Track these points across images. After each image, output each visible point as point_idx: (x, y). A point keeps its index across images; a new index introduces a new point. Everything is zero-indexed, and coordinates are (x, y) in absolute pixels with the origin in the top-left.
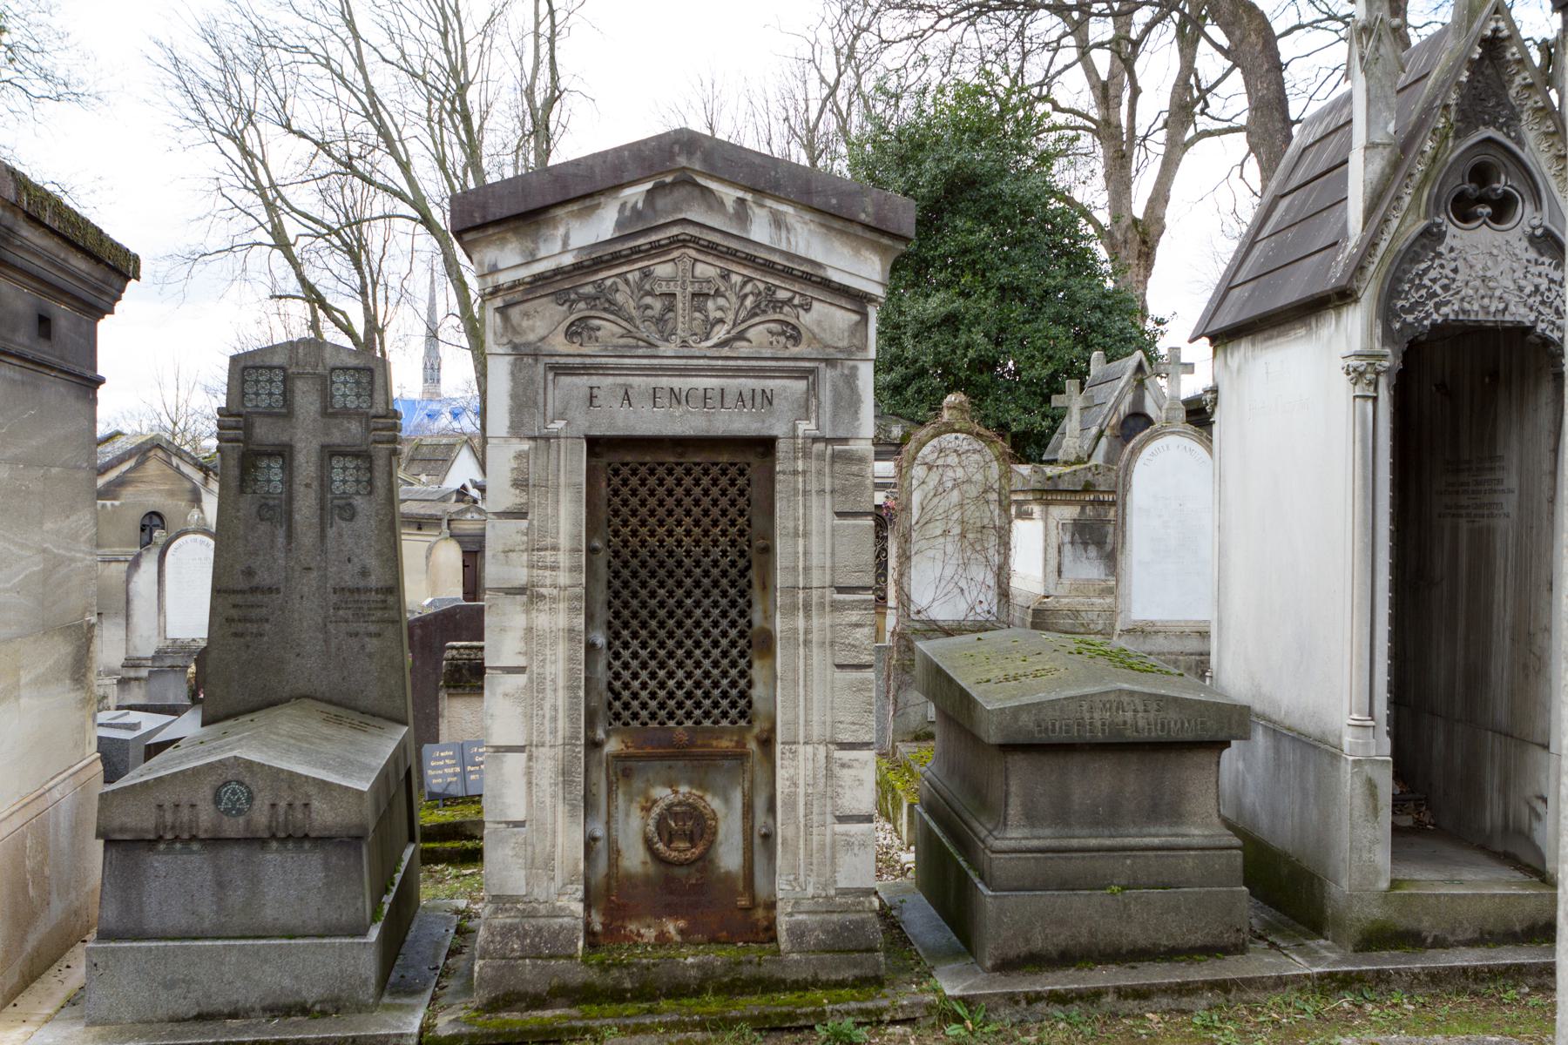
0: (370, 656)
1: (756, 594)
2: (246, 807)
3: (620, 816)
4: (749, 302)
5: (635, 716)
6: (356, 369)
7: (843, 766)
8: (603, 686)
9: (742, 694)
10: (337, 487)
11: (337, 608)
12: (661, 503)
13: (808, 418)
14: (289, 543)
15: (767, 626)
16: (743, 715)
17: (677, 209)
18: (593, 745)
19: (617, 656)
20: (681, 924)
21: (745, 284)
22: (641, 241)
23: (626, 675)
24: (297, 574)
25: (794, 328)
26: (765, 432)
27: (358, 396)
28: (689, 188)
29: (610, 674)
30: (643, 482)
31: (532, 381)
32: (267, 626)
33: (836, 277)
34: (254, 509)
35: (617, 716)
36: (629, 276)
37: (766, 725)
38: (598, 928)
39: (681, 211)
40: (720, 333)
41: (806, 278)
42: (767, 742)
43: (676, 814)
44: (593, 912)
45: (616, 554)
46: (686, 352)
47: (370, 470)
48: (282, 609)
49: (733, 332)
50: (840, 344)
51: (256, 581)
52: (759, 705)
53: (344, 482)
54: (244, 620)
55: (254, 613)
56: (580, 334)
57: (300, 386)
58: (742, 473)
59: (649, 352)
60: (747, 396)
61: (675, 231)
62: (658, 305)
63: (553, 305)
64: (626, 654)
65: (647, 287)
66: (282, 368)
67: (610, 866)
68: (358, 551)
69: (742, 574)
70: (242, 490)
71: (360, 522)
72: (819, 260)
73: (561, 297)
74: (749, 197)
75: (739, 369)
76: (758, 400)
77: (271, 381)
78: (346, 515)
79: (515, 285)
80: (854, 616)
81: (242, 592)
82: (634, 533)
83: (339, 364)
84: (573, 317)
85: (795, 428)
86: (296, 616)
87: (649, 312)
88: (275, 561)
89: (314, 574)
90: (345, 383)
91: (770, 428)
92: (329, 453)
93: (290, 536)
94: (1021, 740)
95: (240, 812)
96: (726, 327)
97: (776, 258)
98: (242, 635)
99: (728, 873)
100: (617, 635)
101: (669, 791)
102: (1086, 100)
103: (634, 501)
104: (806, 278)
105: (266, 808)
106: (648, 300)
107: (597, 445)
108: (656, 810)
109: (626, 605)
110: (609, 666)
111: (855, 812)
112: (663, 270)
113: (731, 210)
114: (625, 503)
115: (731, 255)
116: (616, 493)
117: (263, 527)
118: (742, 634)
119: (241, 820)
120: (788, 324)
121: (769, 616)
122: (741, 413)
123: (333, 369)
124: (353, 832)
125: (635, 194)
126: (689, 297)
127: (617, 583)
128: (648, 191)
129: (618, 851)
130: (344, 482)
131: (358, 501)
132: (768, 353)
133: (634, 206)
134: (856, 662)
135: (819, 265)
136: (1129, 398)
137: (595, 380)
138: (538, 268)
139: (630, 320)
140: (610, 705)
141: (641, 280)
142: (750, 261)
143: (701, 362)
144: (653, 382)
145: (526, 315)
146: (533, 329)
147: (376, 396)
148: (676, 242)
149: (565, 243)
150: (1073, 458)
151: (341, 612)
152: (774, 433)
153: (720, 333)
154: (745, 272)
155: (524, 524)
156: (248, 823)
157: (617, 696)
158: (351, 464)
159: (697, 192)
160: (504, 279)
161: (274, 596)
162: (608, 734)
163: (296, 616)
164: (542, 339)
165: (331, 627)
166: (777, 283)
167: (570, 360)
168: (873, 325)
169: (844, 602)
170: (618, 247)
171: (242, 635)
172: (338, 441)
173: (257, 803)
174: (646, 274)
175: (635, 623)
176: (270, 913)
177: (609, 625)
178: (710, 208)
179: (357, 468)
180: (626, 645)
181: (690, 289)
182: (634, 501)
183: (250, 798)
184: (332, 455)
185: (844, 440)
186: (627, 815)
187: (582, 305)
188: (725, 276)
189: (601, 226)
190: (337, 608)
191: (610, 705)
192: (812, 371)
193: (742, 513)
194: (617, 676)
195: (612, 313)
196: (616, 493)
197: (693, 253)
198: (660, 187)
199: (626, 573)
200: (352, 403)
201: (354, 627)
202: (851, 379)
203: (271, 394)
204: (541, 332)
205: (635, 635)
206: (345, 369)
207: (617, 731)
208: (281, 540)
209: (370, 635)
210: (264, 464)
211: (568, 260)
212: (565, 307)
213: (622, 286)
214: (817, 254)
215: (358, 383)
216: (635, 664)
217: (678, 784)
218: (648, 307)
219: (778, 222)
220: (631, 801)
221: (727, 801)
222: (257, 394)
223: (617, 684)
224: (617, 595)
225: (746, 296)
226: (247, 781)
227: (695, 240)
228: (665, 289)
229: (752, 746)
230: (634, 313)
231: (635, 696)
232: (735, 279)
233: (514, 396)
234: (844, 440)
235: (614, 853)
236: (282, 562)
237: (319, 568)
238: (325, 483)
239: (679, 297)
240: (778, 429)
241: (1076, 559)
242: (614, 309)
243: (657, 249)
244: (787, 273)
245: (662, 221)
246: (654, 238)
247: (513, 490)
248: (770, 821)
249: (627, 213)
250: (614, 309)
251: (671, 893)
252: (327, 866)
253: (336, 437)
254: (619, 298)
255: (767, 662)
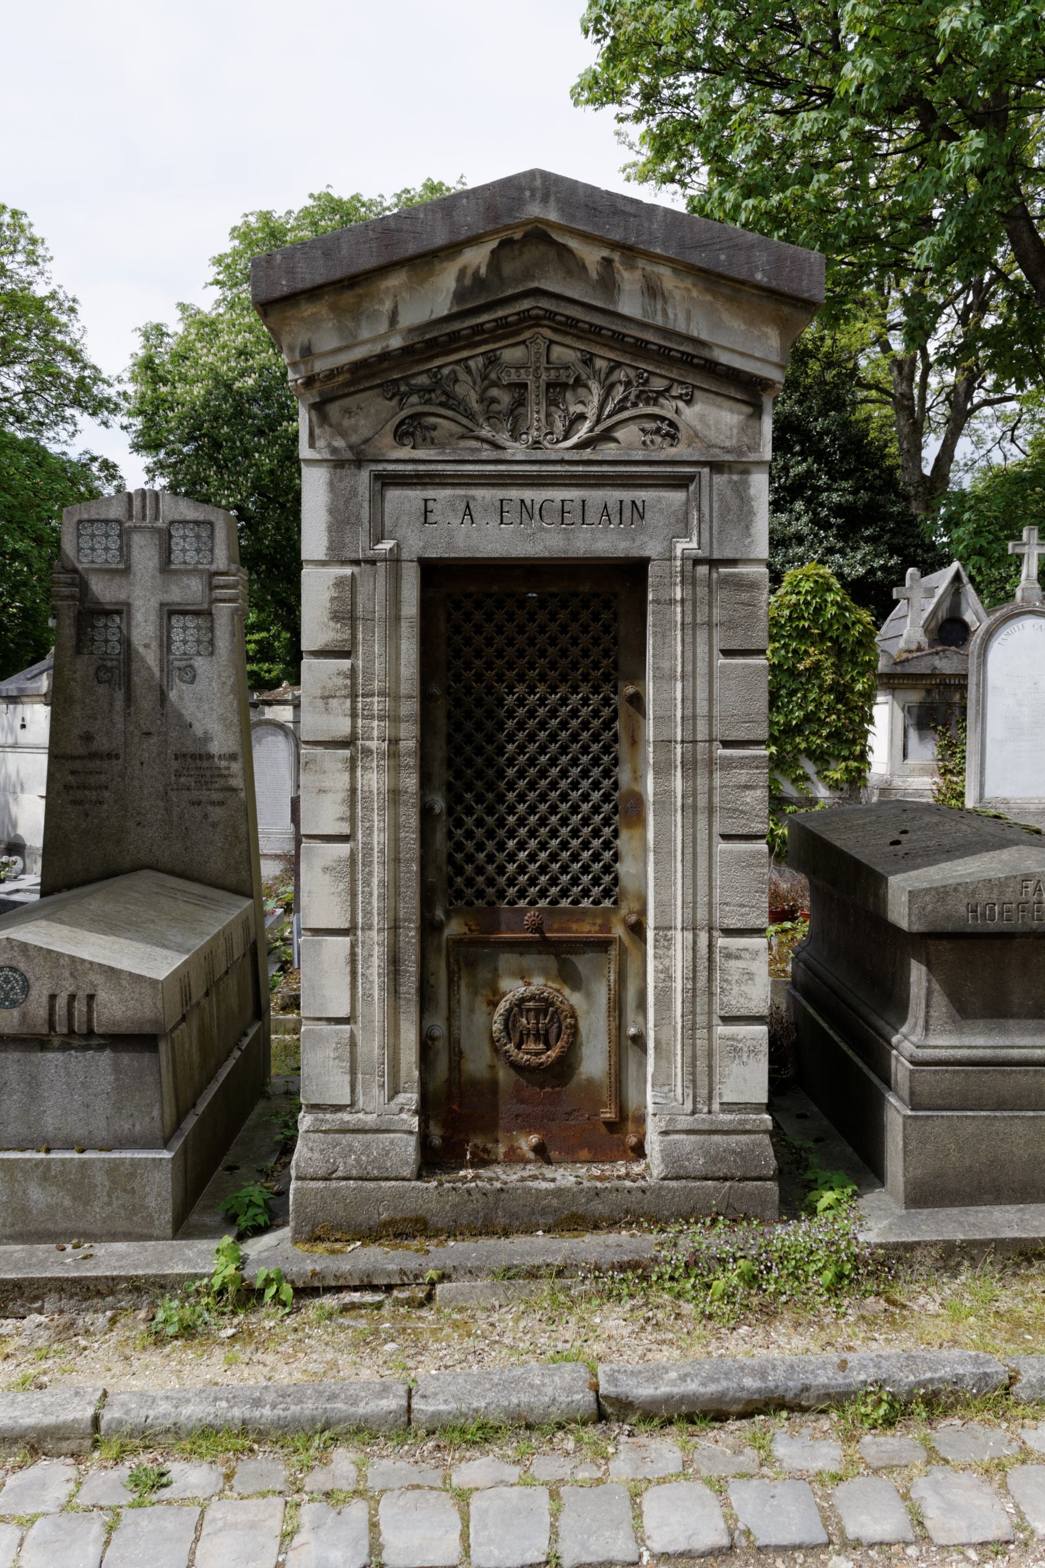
0: (214, 825)
1: (622, 748)
2: (21, 997)
3: (464, 1011)
4: (619, 392)
5: (480, 894)
6: (197, 523)
7: (729, 956)
8: (443, 857)
9: (607, 869)
10: (177, 648)
11: (178, 775)
12: (511, 642)
13: (687, 535)
14: (128, 706)
15: (636, 788)
16: (607, 893)
17: (528, 275)
18: (429, 928)
19: (459, 823)
20: (534, 1139)
21: (611, 370)
22: (484, 318)
23: (470, 845)
24: (136, 740)
25: (672, 424)
26: (635, 553)
27: (198, 551)
28: (543, 248)
29: (451, 844)
30: (489, 617)
31: (354, 492)
32: (107, 794)
33: (724, 358)
34: (92, 671)
35: (459, 894)
36: (471, 363)
37: (636, 906)
38: (437, 1141)
39: (533, 278)
40: (583, 431)
41: (686, 361)
42: (638, 930)
43: (529, 1010)
44: (432, 1123)
45: (458, 703)
46: (539, 455)
47: (211, 629)
48: (122, 776)
49: (598, 429)
50: (727, 444)
51: (95, 746)
52: (626, 881)
53: (185, 642)
54: (84, 787)
55: (92, 780)
56: (413, 434)
57: (137, 540)
58: (607, 605)
59: (494, 455)
60: (613, 509)
61: (526, 304)
62: (506, 399)
63: (380, 400)
64: (469, 821)
65: (493, 376)
66: (118, 522)
67: (451, 1069)
68: (200, 716)
69: (607, 725)
70: (78, 650)
71: (201, 685)
72: (704, 336)
73: (393, 391)
74: (616, 257)
75: (604, 476)
76: (627, 513)
77: (107, 536)
78: (187, 678)
79: (332, 374)
80: (743, 776)
81: (80, 758)
82: (479, 677)
83: (177, 518)
84: (404, 414)
85: (671, 549)
86: (136, 783)
87: (495, 407)
88: (114, 724)
89: (154, 740)
90: (184, 537)
91: (641, 547)
92: (170, 612)
93: (129, 699)
94: (950, 927)
95: (14, 1004)
96: (587, 424)
97: (649, 336)
98: (80, 803)
99: (590, 1081)
100: (459, 799)
101: (521, 983)
102: (886, 377)
103: (479, 640)
104: (686, 361)
105: (44, 1000)
106: (495, 392)
107: (433, 572)
108: (503, 1006)
109: (469, 763)
110: (450, 835)
111: (744, 1012)
112: (512, 355)
113: (594, 276)
114: (468, 642)
115: (594, 333)
116: (457, 630)
117: (102, 690)
118: (606, 798)
119: (16, 1012)
120: (663, 419)
121: (638, 776)
122: (606, 529)
123: (172, 523)
124: (148, 1029)
125: (477, 257)
126: (543, 387)
127: (459, 738)
128: (493, 252)
129: (461, 1053)
130: (185, 642)
131: (199, 663)
132: (639, 455)
133: (476, 272)
134: (745, 831)
135: (703, 344)
136: (946, 605)
137: (430, 493)
138: (358, 354)
139: (471, 416)
140: (450, 882)
141: (486, 367)
142: (617, 341)
143: (558, 468)
144: (500, 493)
145: (348, 412)
146: (355, 430)
147: (216, 551)
148: (528, 320)
149: (393, 320)
150: (914, 647)
151: (183, 779)
152: (647, 553)
153: (583, 431)
154: (612, 356)
155: (345, 664)
156: (24, 1016)
157: (459, 871)
158: (191, 622)
159: (552, 254)
160: (321, 366)
161: (114, 762)
162: (448, 915)
163: (136, 783)
164: (366, 441)
165: (173, 796)
166: (650, 368)
167: (400, 467)
168: (767, 426)
169: (730, 759)
170: (457, 326)
171: (80, 803)
172: (178, 599)
173: (34, 993)
174: (492, 360)
175: (479, 784)
176: (50, 1123)
177: (450, 787)
178: (569, 273)
179: (198, 628)
180: (469, 811)
181: (544, 377)
182: (479, 640)
183: (26, 988)
184: (171, 613)
185: (733, 562)
186: (472, 1010)
187: (414, 399)
188: (588, 360)
189: (435, 298)
190: (178, 775)
191: (450, 882)
192: (691, 478)
193: (606, 654)
194: (459, 847)
195: (450, 408)
196: (457, 630)
197: (548, 333)
198: (502, 244)
199: (469, 725)
200: (191, 557)
201: (195, 795)
202: (742, 494)
203: (107, 549)
204: (365, 432)
205: (480, 799)
206: (185, 522)
207: (458, 912)
208: (119, 704)
209: (213, 803)
210: (101, 624)
211: (396, 342)
212: (394, 402)
213: (463, 376)
214: (700, 330)
215: (198, 537)
216: (479, 832)
217: (530, 975)
218: (494, 400)
219: (652, 290)
220: (476, 993)
221: (589, 996)
222: (93, 549)
223: (459, 856)
224: (458, 751)
225: (612, 386)
226: (22, 966)
227: (551, 315)
228: (514, 378)
229: (619, 931)
230: (476, 407)
231: (480, 870)
232: (600, 364)
233: (332, 511)
234: (733, 562)
235: (457, 1055)
236: (120, 726)
237: (159, 733)
238: (166, 644)
239: (531, 387)
240: (651, 548)
241: (922, 738)
242: (452, 402)
243: (505, 330)
244: (664, 356)
245: (510, 292)
246: (500, 313)
247: (332, 624)
248: (640, 1019)
249: (468, 281)
250: (452, 402)
251: (522, 1101)
252: (117, 1069)
253: (176, 595)
254: (460, 390)
255: (636, 832)
